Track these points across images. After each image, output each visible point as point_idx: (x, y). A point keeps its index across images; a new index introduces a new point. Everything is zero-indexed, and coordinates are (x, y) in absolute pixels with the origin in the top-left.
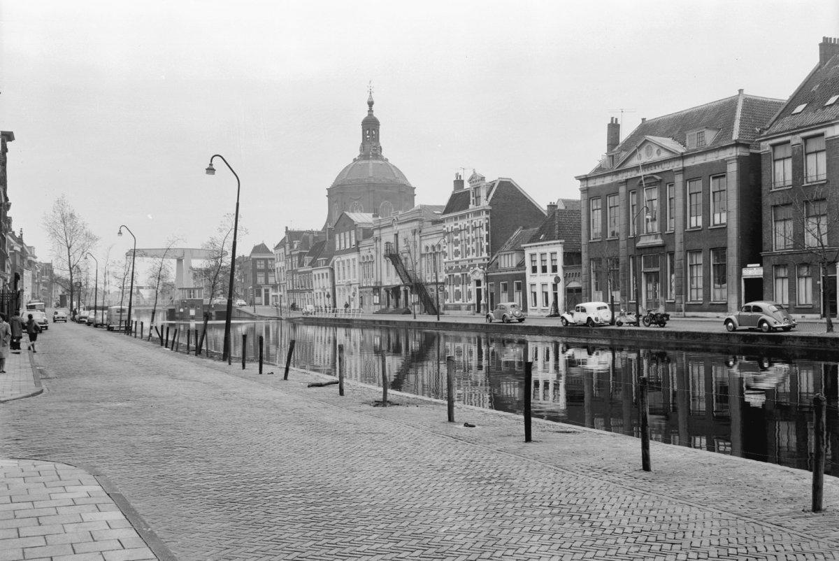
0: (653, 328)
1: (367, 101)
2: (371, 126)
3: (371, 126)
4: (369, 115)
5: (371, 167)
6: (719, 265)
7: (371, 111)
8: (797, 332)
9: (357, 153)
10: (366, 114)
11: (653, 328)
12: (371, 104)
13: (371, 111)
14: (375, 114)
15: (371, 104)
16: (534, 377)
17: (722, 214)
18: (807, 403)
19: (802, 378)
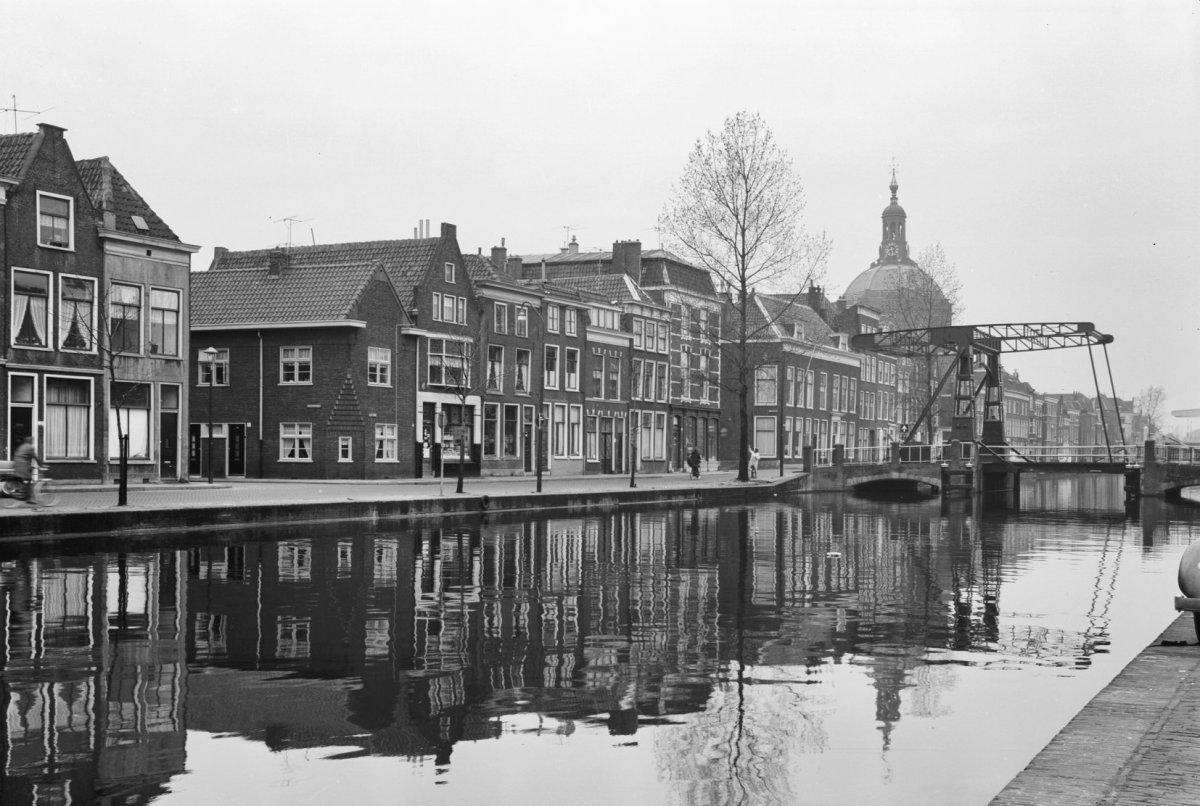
0: (340, 449)
1: (889, 184)
2: (894, 219)
3: (894, 219)
4: (892, 204)
5: (444, 381)
6: (984, 547)
7: (894, 198)
8: (264, 677)
9: (875, 256)
10: (887, 203)
11: (340, 449)
12: (894, 189)
13: (894, 198)
14: (900, 203)
15: (894, 189)
16: (1090, 460)
17: (65, 722)
18: (42, 133)
19: (140, 249)
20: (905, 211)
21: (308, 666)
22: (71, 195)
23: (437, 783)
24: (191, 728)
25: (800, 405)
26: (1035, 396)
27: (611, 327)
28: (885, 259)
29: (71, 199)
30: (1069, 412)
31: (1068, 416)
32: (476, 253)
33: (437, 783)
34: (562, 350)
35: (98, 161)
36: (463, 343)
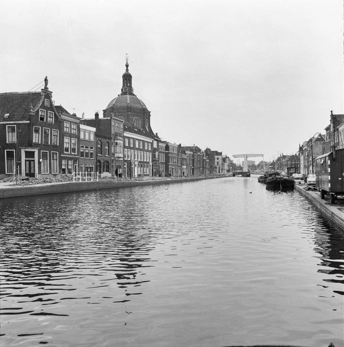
1: (125, 64)
2: (127, 78)
3: (127, 78)
4: (126, 72)
7: (127, 70)
12: (127, 66)
13: (127, 70)
15: (127, 66)
20: (132, 75)
21: (82, 312)
22: (49, 128)
23: (317, 285)
24: (343, 292)
25: (145, 161)
26: (159, 141)
27: (73, 128)
28: (124, 93)
29: (50, 129)
30: (186, 152)
31: (186, 154)
32: (59, 105)
33: (317, 285)
34: (144, 164)
35: (206, 149)
36: (166, 176)
